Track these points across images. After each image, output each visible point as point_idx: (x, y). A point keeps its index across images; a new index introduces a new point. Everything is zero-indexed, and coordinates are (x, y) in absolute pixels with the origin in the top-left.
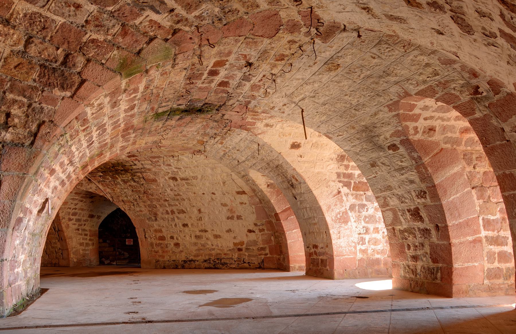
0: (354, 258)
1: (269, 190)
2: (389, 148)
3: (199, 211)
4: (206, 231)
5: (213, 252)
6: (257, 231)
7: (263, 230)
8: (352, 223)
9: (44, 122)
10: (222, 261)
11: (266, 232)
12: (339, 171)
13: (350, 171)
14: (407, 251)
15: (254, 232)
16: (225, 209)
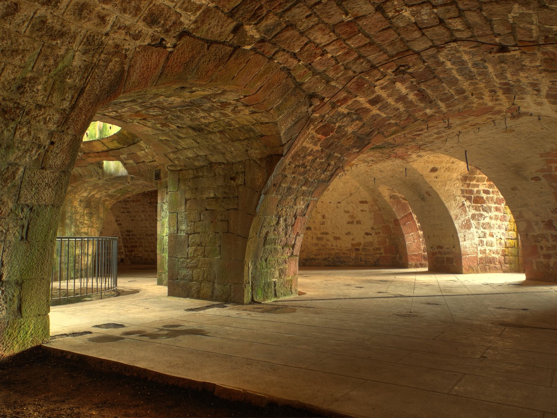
0: (477, 257)
1: (391, 200)
2: (532, 179)
3: (324, 217)
4: (327, 234)
5: (332, 252)
6: (373, 234)
7: (379, 233)
8: (473, 230)
9: (339, 167)
10: (341, 259)
11: (382, 235)
12: (463, 188)
13: (470, 188)
14: (540, 251)
15: (371, 234)
16: (347, 215)
